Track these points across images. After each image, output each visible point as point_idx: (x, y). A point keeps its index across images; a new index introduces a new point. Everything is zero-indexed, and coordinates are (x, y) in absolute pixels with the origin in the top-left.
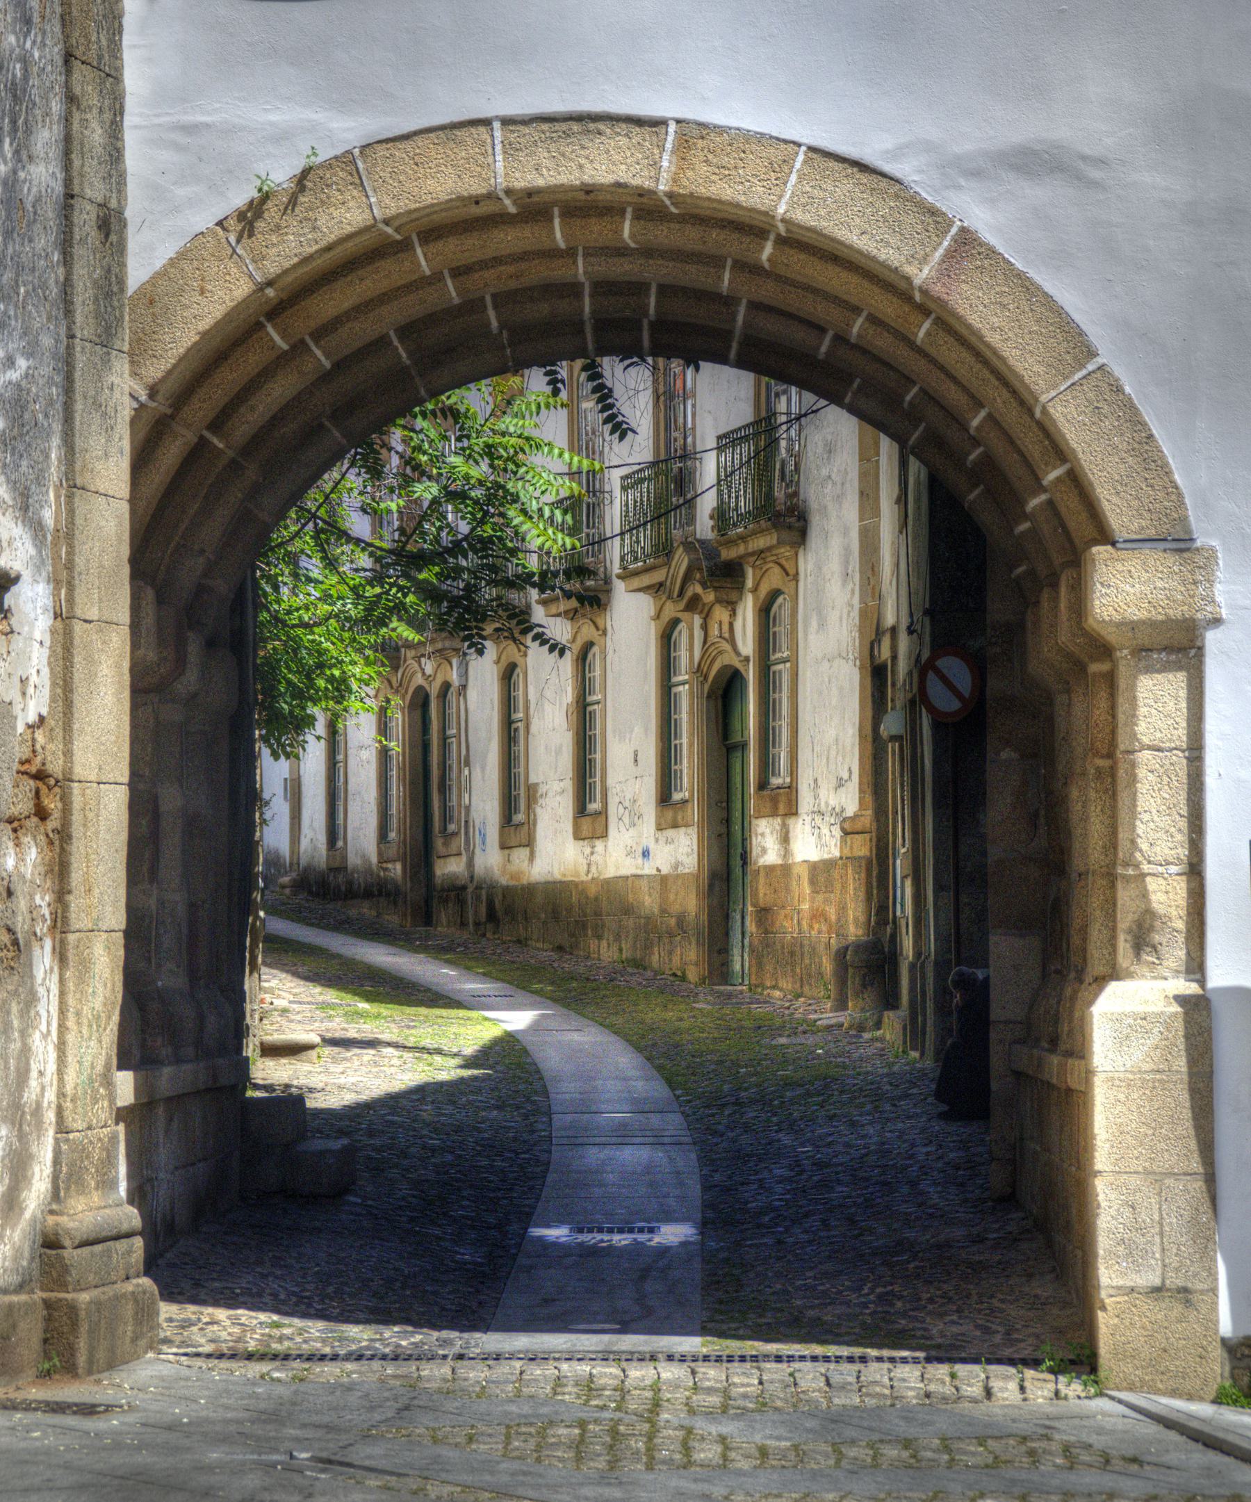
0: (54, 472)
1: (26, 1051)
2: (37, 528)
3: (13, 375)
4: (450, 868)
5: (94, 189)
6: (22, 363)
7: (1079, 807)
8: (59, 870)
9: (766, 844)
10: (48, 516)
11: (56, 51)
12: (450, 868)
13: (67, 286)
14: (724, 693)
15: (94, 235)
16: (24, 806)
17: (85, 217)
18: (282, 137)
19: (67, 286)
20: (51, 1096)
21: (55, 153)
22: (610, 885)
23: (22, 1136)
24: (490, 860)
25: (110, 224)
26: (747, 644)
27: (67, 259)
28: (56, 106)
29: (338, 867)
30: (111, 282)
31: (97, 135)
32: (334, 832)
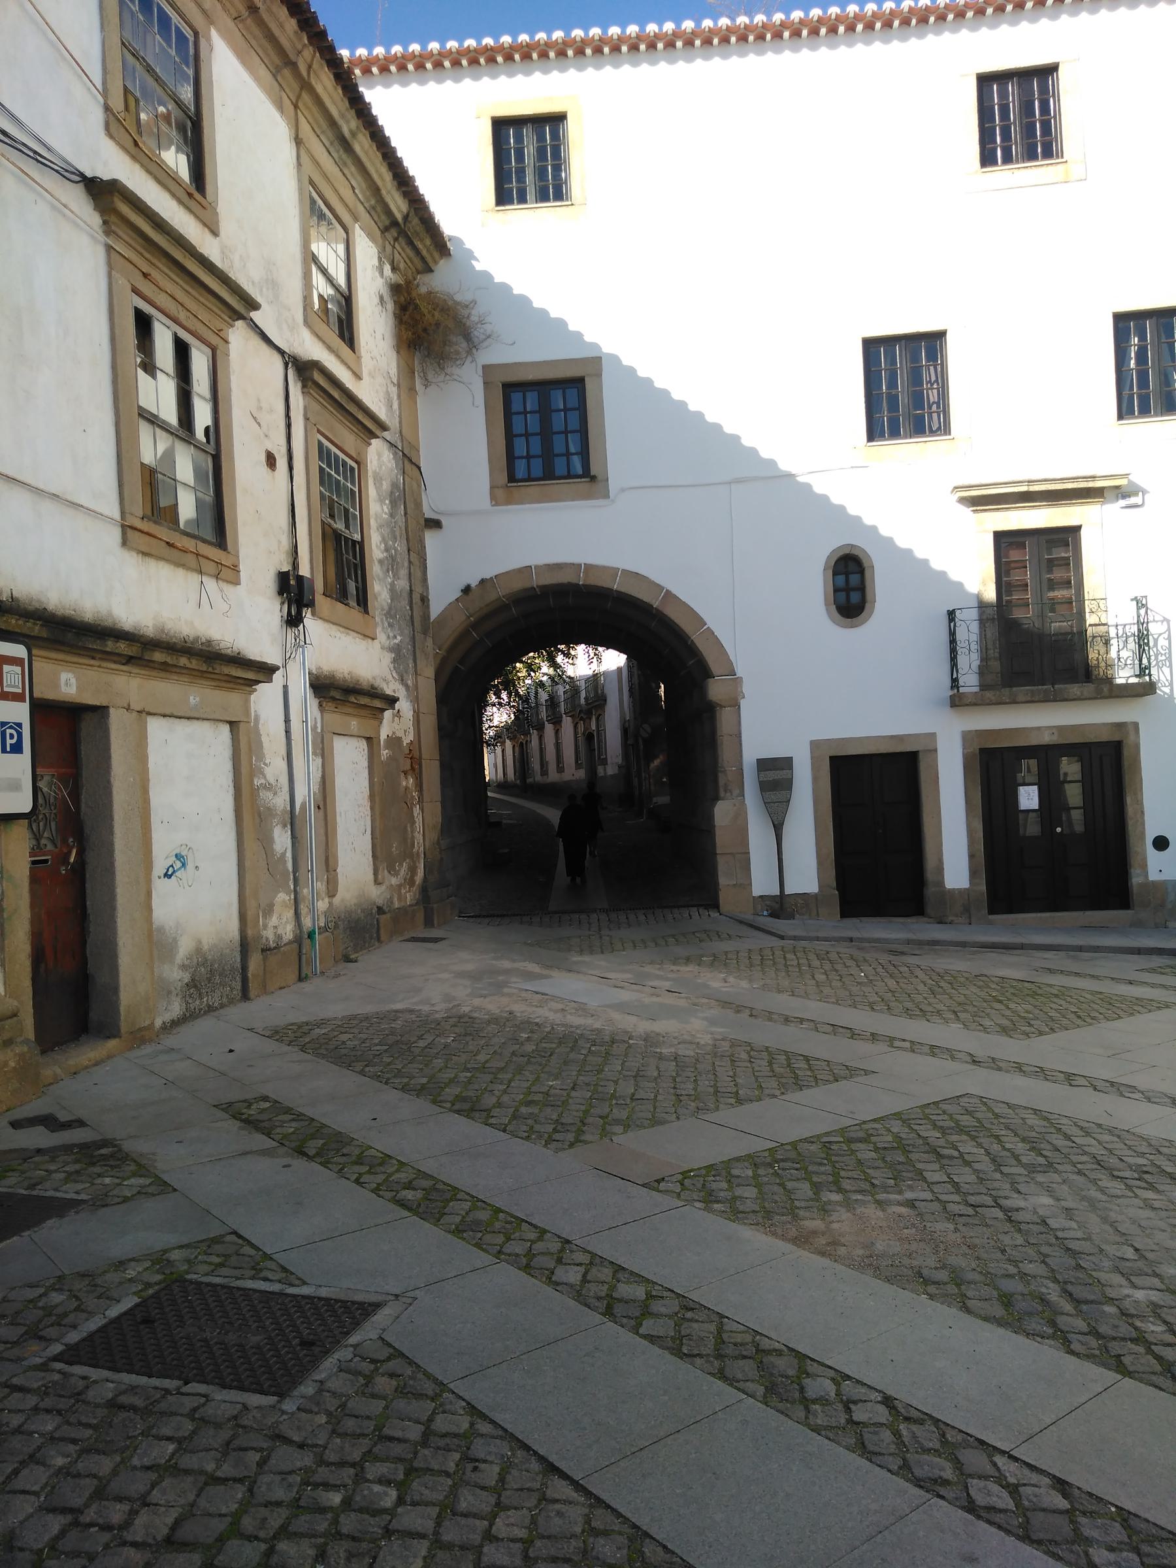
0: (411, 670)
1: (413, 837)
2: (407, 687)
3: (396, 641)
4: (529, 780)
5: (418, 589)
6: (399, 638)
7: (603, 963)
8: (420, 786)
9: (600, 771)
10: (409, 682)
11: (405, 549)
12: (529, 780)
13: (412, 617)
14: (589, 737)
15: (420, 603)
16: (408, 767)
17: (416, 597)
18: (379, 455)
19: (412, 617)
20: (422, 849)
21: (406, 577)
22: (566, 782)
23: (414, 862)
24: (538, 778)
25: (424, 600)
26: (594, 727)
27: (411, 609)
28: (406, 564)
29: (506, 782)
30: (426, 616)
31: (419, 574)
32: (505, 774)
